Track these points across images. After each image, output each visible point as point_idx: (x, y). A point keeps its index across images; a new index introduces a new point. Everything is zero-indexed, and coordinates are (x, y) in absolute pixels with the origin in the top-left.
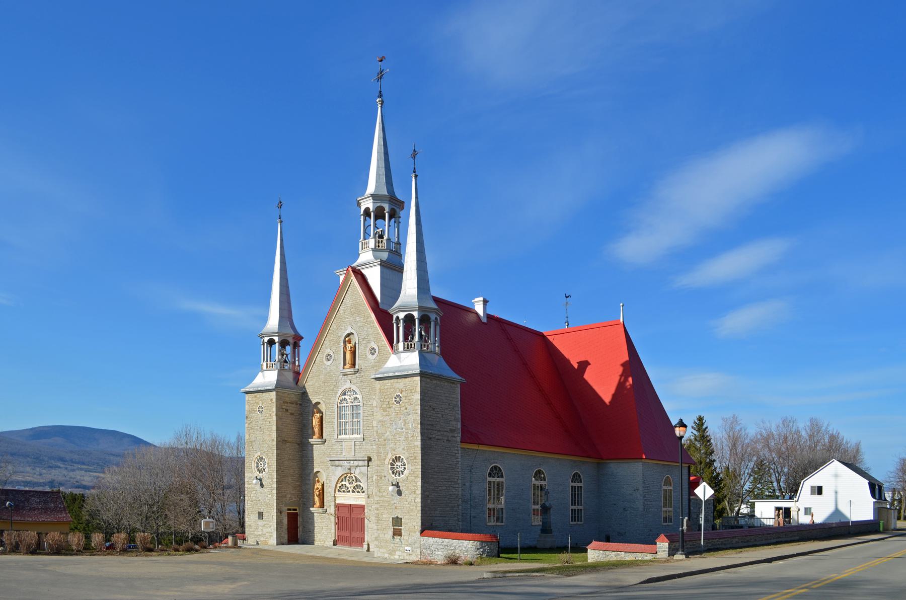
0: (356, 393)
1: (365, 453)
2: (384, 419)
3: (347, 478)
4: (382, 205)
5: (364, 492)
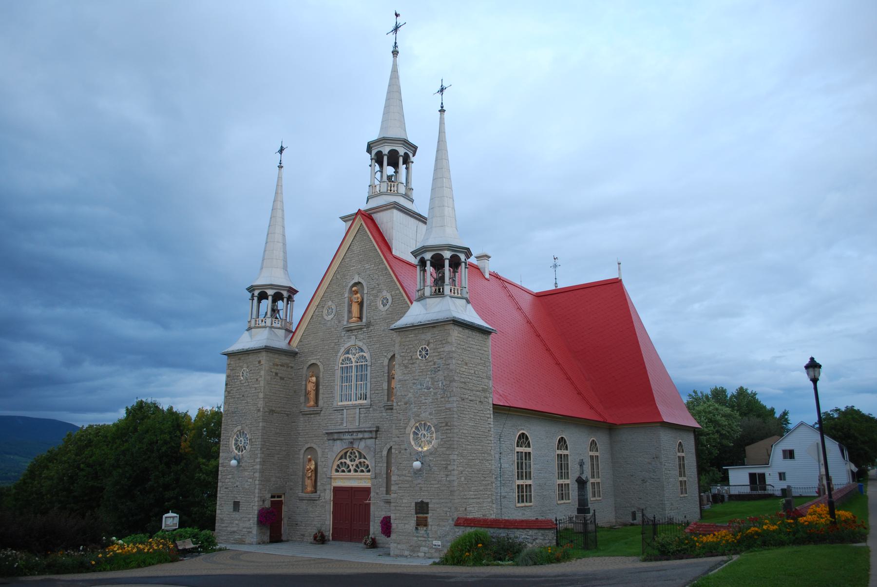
0: (362, 350)
1: (373, 422)
2: (406, 378)
3: (348, 454)
4: (396, 148)
5: (369, 471)
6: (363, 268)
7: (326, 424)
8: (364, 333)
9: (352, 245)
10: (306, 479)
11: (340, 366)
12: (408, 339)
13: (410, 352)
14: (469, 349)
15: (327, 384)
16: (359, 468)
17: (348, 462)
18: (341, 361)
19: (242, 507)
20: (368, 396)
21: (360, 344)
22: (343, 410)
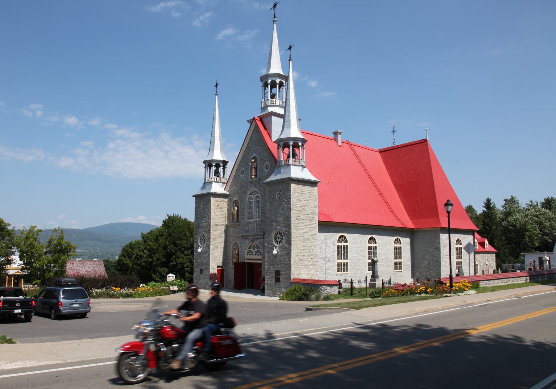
0: (258, 193)
3: (252, 246)
4: (282, 80)
5: (261, 255)
10: (234, 258)
11: (247, 201)
12: (272, 188)
14: (302, 193)
16: (257, 253)
17: (252, 250)
18: (248, 199)
19: (204, 271)
21: (256, 190)
22: (249, 224)
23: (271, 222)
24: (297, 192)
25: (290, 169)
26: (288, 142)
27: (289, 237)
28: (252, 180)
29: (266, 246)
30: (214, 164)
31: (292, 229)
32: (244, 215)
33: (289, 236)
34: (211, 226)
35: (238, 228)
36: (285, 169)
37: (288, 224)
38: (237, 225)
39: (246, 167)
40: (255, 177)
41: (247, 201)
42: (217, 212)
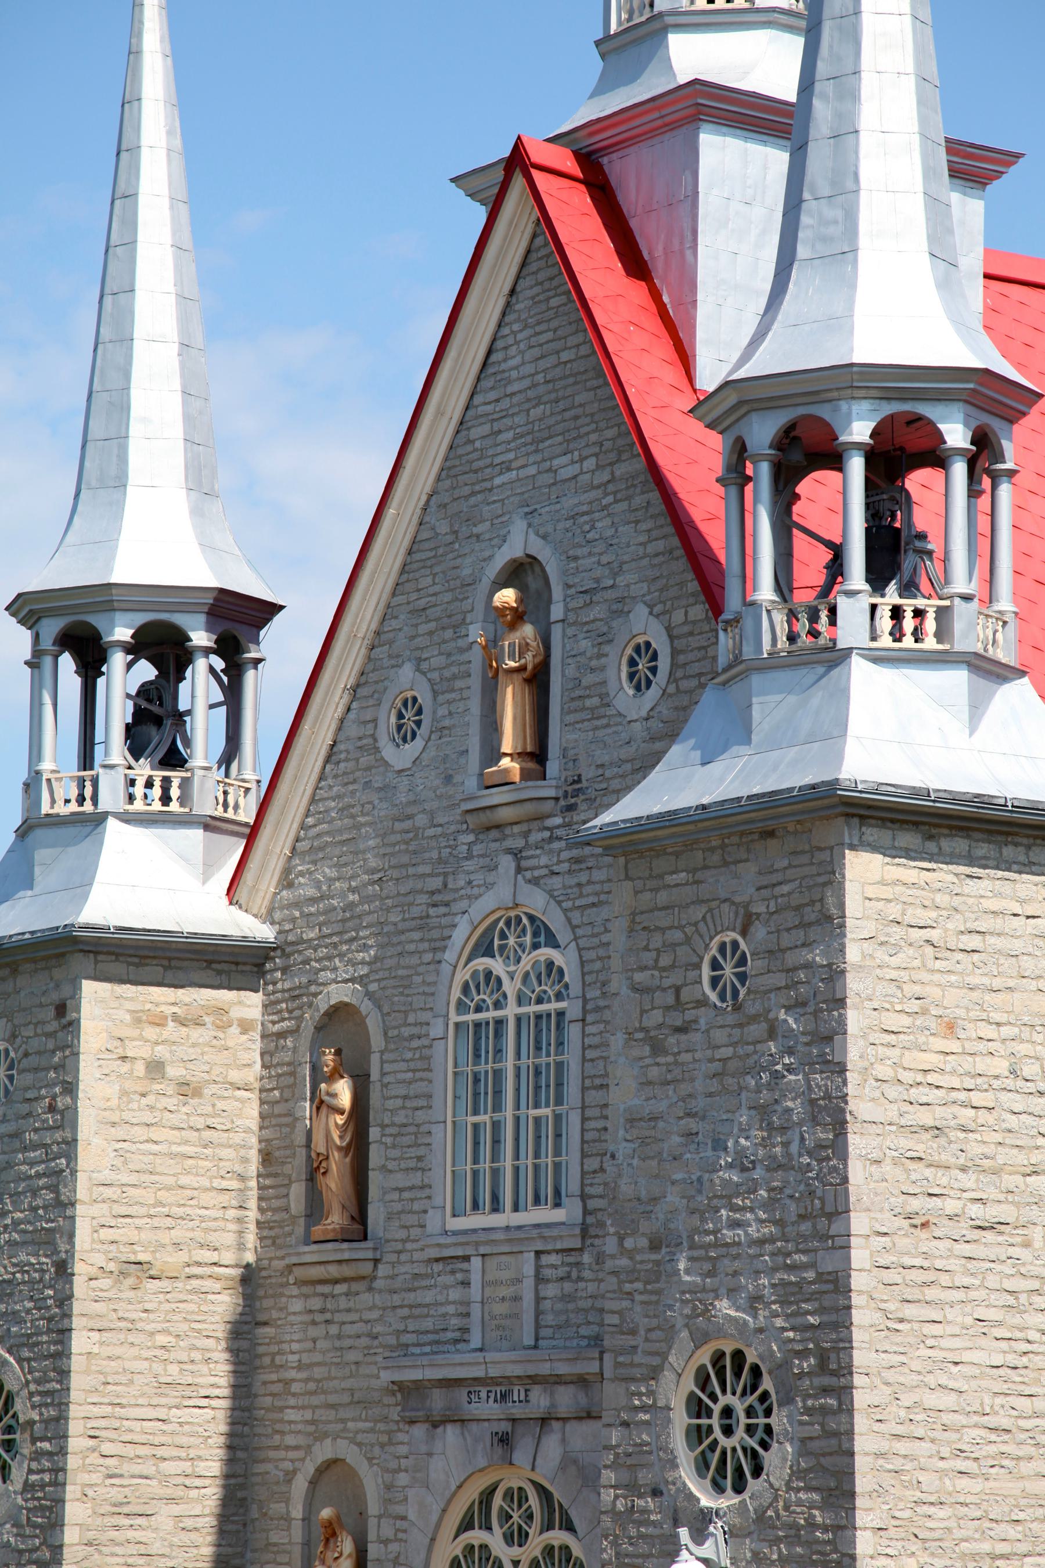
0: (552, 942)
3: (498, 1501)
6: (548, 478)
7: (398, 1333)
8: (551, 839)
9: (500, 344)
11: (454, 1018)
12: (663, 897)
13: (673, 966)
14: (974, 942)
15: (400, 1119)
18: (456, 993)
20: (572, 1183)
21: (535, 901)
22: (466, 1258)
23: (655, 1245)
24: (916, 934)
25: (843, 694)
26: (824, 412)
27: (824, 1410)
28: (497, 796)
29: (613, 1512)
30: (123, 633)
31: (857, 1335)
32: (421, 1165)
33: (832, 1402)
34: (80, 1286)
35: (366, 1298)
36: (792, 699)
37: (820, 1277)
38: (347, 1271)
39: (438, 661)
40: (525, 775)
41: (454, 1018)
42: (140, 1133)
